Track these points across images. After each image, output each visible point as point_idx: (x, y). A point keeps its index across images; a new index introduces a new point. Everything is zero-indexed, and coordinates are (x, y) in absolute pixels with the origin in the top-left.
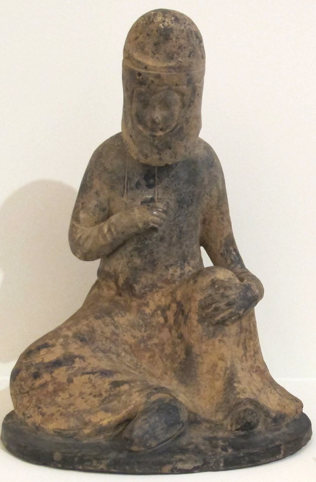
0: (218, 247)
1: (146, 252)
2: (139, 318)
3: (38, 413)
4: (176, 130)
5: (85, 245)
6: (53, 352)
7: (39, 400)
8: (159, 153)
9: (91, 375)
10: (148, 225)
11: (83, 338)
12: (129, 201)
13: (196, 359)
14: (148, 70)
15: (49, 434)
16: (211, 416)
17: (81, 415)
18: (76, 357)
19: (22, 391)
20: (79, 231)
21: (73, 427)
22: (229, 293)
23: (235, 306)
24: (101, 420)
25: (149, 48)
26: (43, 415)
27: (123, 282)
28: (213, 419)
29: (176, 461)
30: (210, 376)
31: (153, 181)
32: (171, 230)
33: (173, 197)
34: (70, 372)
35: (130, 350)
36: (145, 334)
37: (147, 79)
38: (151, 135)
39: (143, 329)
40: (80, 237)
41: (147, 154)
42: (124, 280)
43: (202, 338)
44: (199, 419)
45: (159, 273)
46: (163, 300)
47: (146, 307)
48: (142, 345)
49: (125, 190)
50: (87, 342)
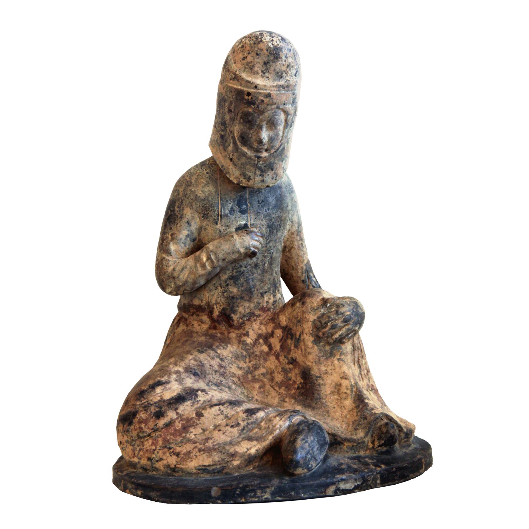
0: (300, 274)
1: (242, 280)
2: (241, 348)
3: (170, 454)
4: (280, 150)
5: (181, 277)
6: (170, 389)
7: (166, 441)
8: (261, 175)
9: (221, 406)
10: (250, 249)
11: (195, 372)
12: (224, 228)
13: (317, 381)
14: (258, 90)
15: (191, 473)
16: (352, 435)
17: (224, 448)
18: (197, 390)
19: (141, 435)
20: (171, 263)
21: (219, 461)
22: (343, 310)
23: (351, 323)
24: (248, 450)
26: (178, 455)
27: (218, 314)
28: (354, 437)
29: (339, 481)
30: (336, 397)
31: (245, 206)
32: (263, 256)
33: (264, 222)
34: (196, 406)
35: (239, 382)
36: (250, 365)
37: (257, 98)
38: (256, 156)
39: (247, 360)
40: (174, 269)
41: (250, 176)
42: (219, 312)
43: (319, 360)
44: (339, 439)
45: (256, 300)
46: (263, 327)
47: (246, 337)
48: (250, 376)
49: (219, 216)
50: (200, 376)
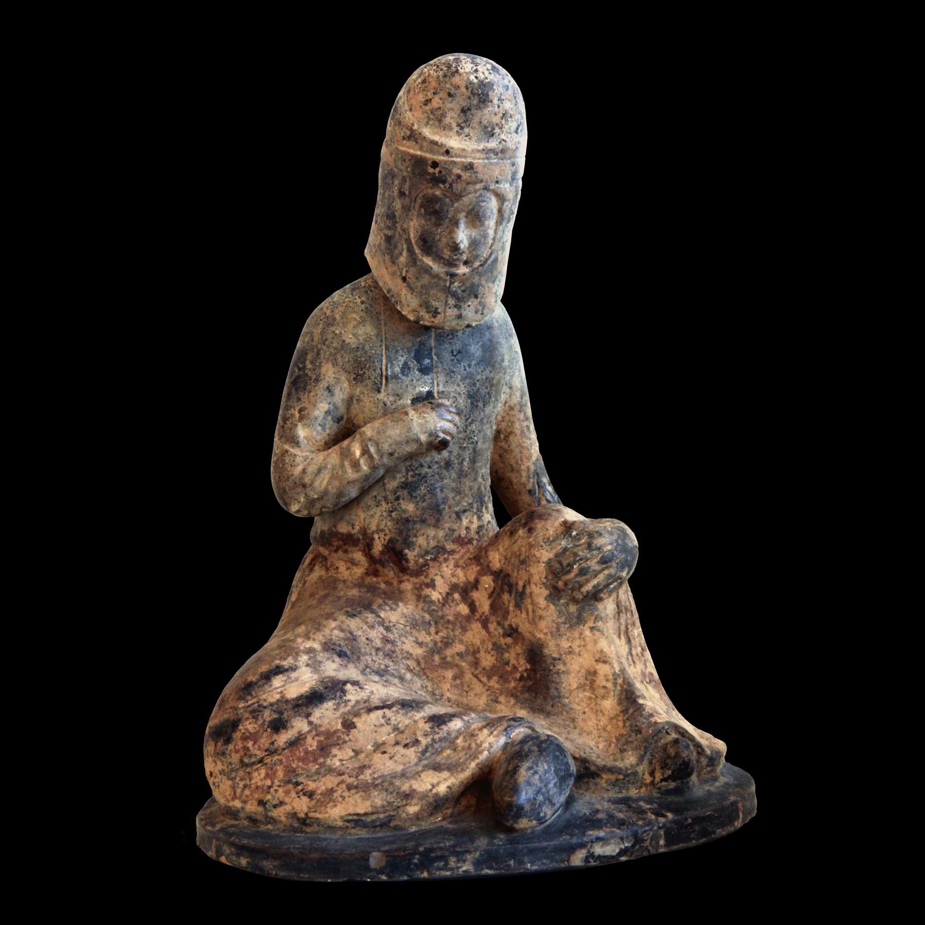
0: (524, 479)
1: (423, 489)
2: (422, 609)
3: (297, 793)
4: (489, 262)
5: (317, 484)
7: (290, 771)
8: (457, 306)
9: (386, 711)
10: (438, 436)
11: (341, 651)
12: (391, 399)
13: (554, 666)
14: (452, 157)
15: (335, 827)
16: (615, 760)
17: (391, 783)
18: (345, 683)
19: (246, 760)
20: (298, 460)
21: (383, 807)
23: (614, 564)
24: (433, 786)
25: (451, 118)
26: (310, 795)
27: (381, 549)
28: (620, 764)
29: (592, 842)
30: (587, 694)
32: (460, 447)
33: (462, 389)
34: (343, 710)
35: (418, 669)
36: (438, 638)
37: (450, 172)
38: (447, 273)
39: (433, 630)
40: (304, 471)
41: (437, 309)
42: (383, 545)
43: (558, 629)
44: (593, 768)
45: (447, 525)
46: (460, 572)
47: (430, 589)
48: (437, 658)
49: (384, 378)
50: (349, 658)
